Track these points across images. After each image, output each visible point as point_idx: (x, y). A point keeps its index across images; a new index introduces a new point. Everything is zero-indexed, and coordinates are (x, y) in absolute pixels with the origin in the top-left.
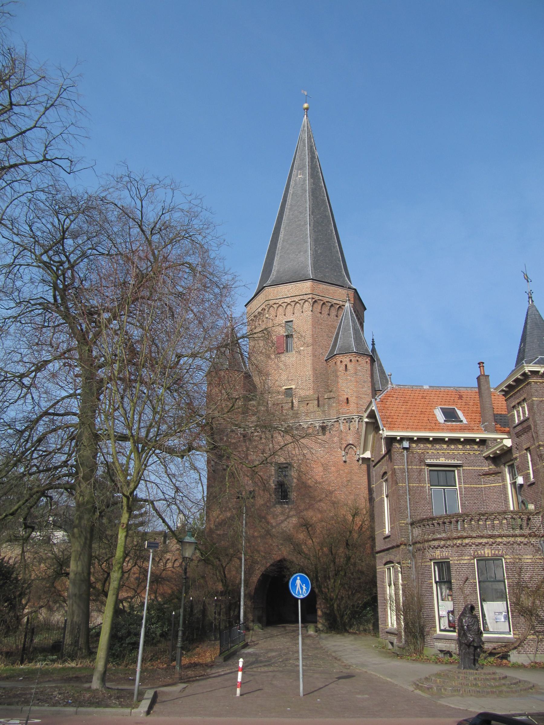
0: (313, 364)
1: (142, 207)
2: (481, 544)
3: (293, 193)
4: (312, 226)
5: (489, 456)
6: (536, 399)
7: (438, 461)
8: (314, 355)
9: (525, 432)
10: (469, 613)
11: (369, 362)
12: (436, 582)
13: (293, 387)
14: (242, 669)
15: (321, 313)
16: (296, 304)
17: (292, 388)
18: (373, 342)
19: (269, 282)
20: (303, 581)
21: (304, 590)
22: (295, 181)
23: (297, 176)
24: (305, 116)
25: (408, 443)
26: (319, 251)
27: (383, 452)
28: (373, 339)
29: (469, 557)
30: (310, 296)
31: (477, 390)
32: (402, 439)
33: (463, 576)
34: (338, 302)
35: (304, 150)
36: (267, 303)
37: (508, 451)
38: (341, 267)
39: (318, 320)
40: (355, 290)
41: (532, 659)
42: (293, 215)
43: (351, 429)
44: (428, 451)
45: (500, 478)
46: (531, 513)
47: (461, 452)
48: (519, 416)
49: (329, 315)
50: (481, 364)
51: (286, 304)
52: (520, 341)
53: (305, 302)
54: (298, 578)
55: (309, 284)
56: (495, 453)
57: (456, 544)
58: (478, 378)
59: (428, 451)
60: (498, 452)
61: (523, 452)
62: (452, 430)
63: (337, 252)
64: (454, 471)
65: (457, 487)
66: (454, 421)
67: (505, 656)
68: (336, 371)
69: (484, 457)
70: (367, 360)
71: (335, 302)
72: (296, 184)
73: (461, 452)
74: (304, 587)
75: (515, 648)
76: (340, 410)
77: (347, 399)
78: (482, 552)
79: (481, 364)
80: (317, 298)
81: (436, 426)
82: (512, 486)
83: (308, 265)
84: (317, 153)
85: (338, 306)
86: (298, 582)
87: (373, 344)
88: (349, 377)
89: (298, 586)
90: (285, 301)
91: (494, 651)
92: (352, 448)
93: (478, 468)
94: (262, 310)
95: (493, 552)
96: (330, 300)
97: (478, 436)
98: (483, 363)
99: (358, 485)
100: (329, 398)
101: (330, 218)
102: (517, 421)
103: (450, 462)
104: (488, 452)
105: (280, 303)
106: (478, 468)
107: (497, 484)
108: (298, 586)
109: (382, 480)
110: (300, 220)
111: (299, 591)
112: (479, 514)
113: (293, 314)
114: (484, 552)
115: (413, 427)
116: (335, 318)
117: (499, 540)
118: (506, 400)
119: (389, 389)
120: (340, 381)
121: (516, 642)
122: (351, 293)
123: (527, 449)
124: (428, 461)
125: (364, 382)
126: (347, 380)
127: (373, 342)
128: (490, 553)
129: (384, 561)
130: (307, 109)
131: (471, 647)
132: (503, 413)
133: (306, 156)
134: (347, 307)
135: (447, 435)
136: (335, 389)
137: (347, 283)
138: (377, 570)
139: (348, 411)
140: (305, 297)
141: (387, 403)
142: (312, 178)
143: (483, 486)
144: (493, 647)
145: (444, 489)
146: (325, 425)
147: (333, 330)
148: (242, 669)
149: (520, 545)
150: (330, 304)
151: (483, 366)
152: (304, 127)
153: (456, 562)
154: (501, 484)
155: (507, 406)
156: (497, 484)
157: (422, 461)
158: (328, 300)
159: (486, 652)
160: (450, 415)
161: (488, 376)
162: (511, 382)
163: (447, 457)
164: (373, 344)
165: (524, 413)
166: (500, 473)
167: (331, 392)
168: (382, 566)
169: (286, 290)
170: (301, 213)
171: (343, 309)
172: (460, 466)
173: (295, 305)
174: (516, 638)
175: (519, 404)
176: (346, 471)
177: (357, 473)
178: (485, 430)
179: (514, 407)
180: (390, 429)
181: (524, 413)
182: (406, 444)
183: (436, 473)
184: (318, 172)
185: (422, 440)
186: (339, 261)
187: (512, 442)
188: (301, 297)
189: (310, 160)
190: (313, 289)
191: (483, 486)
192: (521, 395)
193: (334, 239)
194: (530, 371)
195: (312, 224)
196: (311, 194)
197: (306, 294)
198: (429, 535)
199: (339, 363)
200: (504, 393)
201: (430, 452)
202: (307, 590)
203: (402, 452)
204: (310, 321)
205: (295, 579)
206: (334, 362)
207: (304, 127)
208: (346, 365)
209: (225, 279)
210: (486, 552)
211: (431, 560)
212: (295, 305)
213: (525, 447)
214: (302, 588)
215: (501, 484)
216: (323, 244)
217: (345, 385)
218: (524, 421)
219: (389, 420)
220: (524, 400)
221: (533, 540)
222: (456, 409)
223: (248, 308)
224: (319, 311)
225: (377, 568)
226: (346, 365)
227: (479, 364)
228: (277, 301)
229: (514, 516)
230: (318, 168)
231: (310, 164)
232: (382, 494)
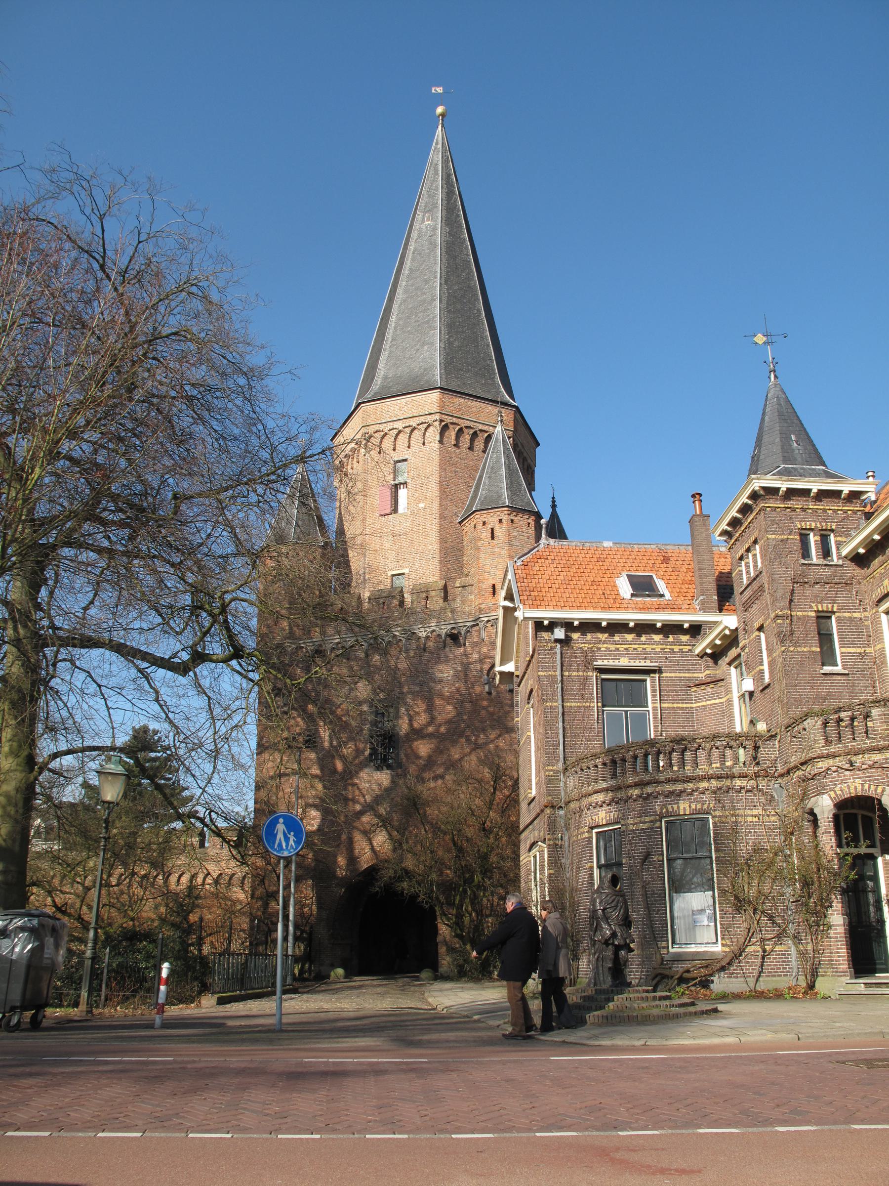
1: (103, 230)
2: (672, 793)
3: (415, 250)
4: (444, 302)
6: (773, 536)
7: (616, 663)
8: (442, 517)
10: (608, 887)
11: (533, 523)
12: (600, 867)
13: (406, 571)
14: (167, 982)
18: (554, 502)
19: (368, 396)
21: (291, 842)
22: (420, 230)
24: (440, 127)
25: (563, 630)
26: (456, 344)
28: (553, 498)
29: (652, 818)
30: (437, 417)
33: (639, 852)
35: (435, 181)
36: (363, 430)
37: (732, 639)
38: (493, 370)
39: (451, 458)
41: (752, 985)
44: (600, 646)
45: (722, 689)
46: (761, 737)
47: (658, 648)
48: (748, 572)
52: (754, 444)
54: (281, 820)
55: (435, 395)
56: (712, 645)
57: (632, 795)
59: (600, 646)
60: (718, 642)
61: (754, 635)
62: (644, 609)
63: (488, 345)
64: (646, 680)
65: (650, 708)
66: (648, 596)
67: (705, 983)
68: (476, 539)
70: (530, 521)
71: (481, 427)
72: (419, 237)
73: (658, 648)
75: (723, 969)
78: (675, 807)
80: (449, 420)
81: (617, 602)
83: (434, 366)
87: (554, 506)
88: (497, 550)
89: (280, 836)
90: (395, 426)
91: (686, 975)
93: (687, 675)
95: (693, 806)
96: (471, 424)
97: (686, 618)
98: (700, 495)
101: (476, 291)
103: (637, 663)
104: (702, 645)
106: (687, 675)
107: (718, 701)
109: (527, 706)
110: (425, 294)
111: (280, 844)
112: (671, 741)
113: (409, 447)
114: (678, 807)
115: (574, 604)
117: (705, 784)
119: (541, 546)
120: (482, 556)
121: (724, 957)
122: (508, 415)
123: (760, 629)
124: (599, 663)
126: (493, 553)
127: (554, 502)
128: (687, 808)
130: (443, 115)
131: (610, 947)
133: (438, 190)
135: (632, 617)
140: (429, 419)
142: (447, 225)
143: (695, 705)
144: (685, 969)
145: (626, 712)
148: (167, 982)
149: (740, 792)
150: (472, 432)
152: (437, 143)
153: (631, 827)
156: (718, 701)
157: (587, 664)
158: (468, 424)
159: (672, 977)
160: (643, 586)
163: (636, 656)
164: (554, 506)
165: (755, 566)
166: (723, 680)
167: (467, 575)
169: (397, 408)
170: (426, 282)
172: (654, 672)
174: (725, 952)
175: (748, 550)
178: (700, 610)
179: (741, 558)
180: (534, 606)
181: (755, 566)
182: (559, 633)
183: (614, 683)
184: (458, 216)
185: (588, 627)
186: (491, 360)
188: (422, 419)
190: (442, 404)
191: (695, 705)
192: (751, 534)
194: (764, 488)
198: (589, 785)
199: (480, 526)
201: (603, 647)
202: (297, 843)
203: (552, 648)
204: (437, 459)
207: (437, 143)
208: (492, 529)
209: (256, 359)
210: (681, 807)
211: (592, 828)
213: (756, 625)
214: (287, 839)
215: (723, 700)
216: (463, 332)
217: (489, 562)
220: (755, 542)
221: (762, 783)
222: (654, 577)
224: (453, 442)
226: (492, 529)
227: (693, 496)
228: (381, 427)
229: (732, 743)
230: (459, 210)
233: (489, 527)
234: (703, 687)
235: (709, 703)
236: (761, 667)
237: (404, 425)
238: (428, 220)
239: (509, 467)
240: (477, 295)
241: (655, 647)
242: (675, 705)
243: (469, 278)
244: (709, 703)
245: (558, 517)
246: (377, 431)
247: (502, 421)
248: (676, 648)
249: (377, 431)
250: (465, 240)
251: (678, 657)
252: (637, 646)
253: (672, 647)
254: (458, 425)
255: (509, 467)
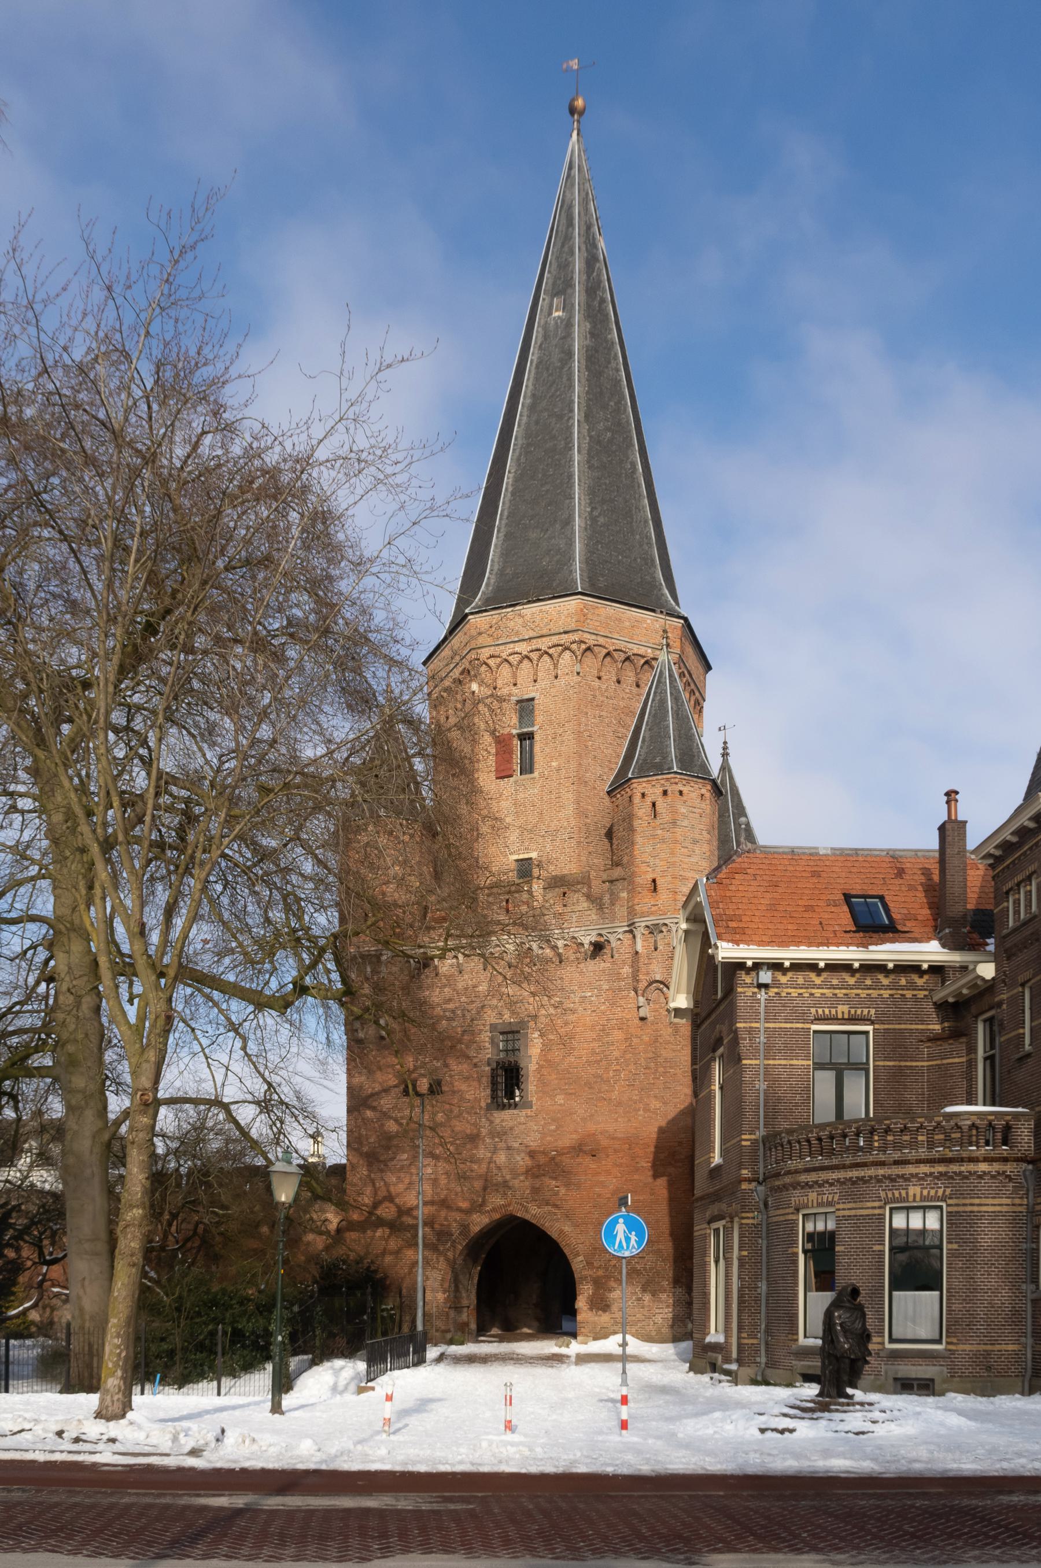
0: (578, 802)
5: (947, 1001)
9: (1025, 947)
11: (708, 795)
15: (599, 678)
16: (541, 656)
17: (531, 859)
18: (725, 748)
20: (631, 1226)
21: (633, 1242)
23: (550, 313)
24: (575, 133)
26: (601, 520)
27: (720, 995)
28: (725, 743)
30: (575, 637)
31: (937, 855)
32: (757, 966)
34: (642, 651)
38: (653, 561)
40: (686, 619)
42: (537, 423)
43: (660, 947)
44: (813, 991)
47: (886, 994)
48: (1017, 912)
49: (619, 682)
50: (951, 796)
51: (517, 657)
53: (563, 651)
54: (621, 1220)
58: (942, 829)
59: (813, 991)
60: (965, 991)
63: (646, 521)
69: (935, 1004)
73: (886, 994)
74: (633, 1238)
76: (636, 907)
77: (654, 881)
79: (951, 796)
80: (591, 640)
82: (988, 1062)
84: (602, 244)
85: (642, 661)
86: (621, 1228)
87: (725, 755)
88: (659, 832)
89: (621, 1236)
90: (517, 649)
92: (661, 990)
94: (462, 673)
98: (957, 793)
99: (671, 1068)
100: (611, 882)
102: (1011, 924)
105: (504, 655)
107: (957, 1060)
108: (621, 1236)
114: (907, 1194)
116: (635, 689)
118: (993, 878)
125: (695, 842)
126: (654, 836)
129: (708, 1214)
132: (989, 907)
134: (663, 662)
136: (625, 859)
137: (667, 601)
138: (695, 1234)
139: (654, 909)
140: (565, 639)
141: (733, 888)
146: (602, 940)
147: (628, 720)
151: (957, 801)
154: (964, 1059)
155: (997, 889)
161: (965, 822)
162: (1007, 835)
164: (725, 755)
168: (705, 1226)
171: (652, 667)
173: (539, 660)
176: (646, 1038)
177: (669, 1043)
181: (1029, 905)
184: (603, 301)
186: (650, 544)
187: (997, 970)
188: (555, 640)
189: (583, 265)
193: (639, 486)
195: (585, 446)
196: (583, 362)
197: (566, 632)
199: (637, 799)
200: (991, 861)
202: (639, 1243)
205: (615, 1222)
206: (626, 797)
207: (571, 168)
208: (654, 805)
212: (539, 660)
218: (1025, 923)
219: (732, 924)
223: (432, 666)
225: (695, 1228)
227: (948, 794)
230: (604, 291)
231: (584, 277)
232: (710, 1083)
233: (649, 800)
234: (939, 1043)
235: (945, 1061)
236: (1021, 1031)
237: (529, 648)
238: (557, 310)
239: (678, 715)
240: (631, 438)
241: (882, 992)
242: (903, 1064)
243: (619, 409)
244: (945, 1061)
245: (730, 771)
246: (492, 656)
247: (668, 645)
248: (909, 994)
249: (492, 656)
250: (613, 343)
251: (909, 1005)
252: (859, 991)
253: (904, 992)
254: (604, 647)
255: (678, 715)
